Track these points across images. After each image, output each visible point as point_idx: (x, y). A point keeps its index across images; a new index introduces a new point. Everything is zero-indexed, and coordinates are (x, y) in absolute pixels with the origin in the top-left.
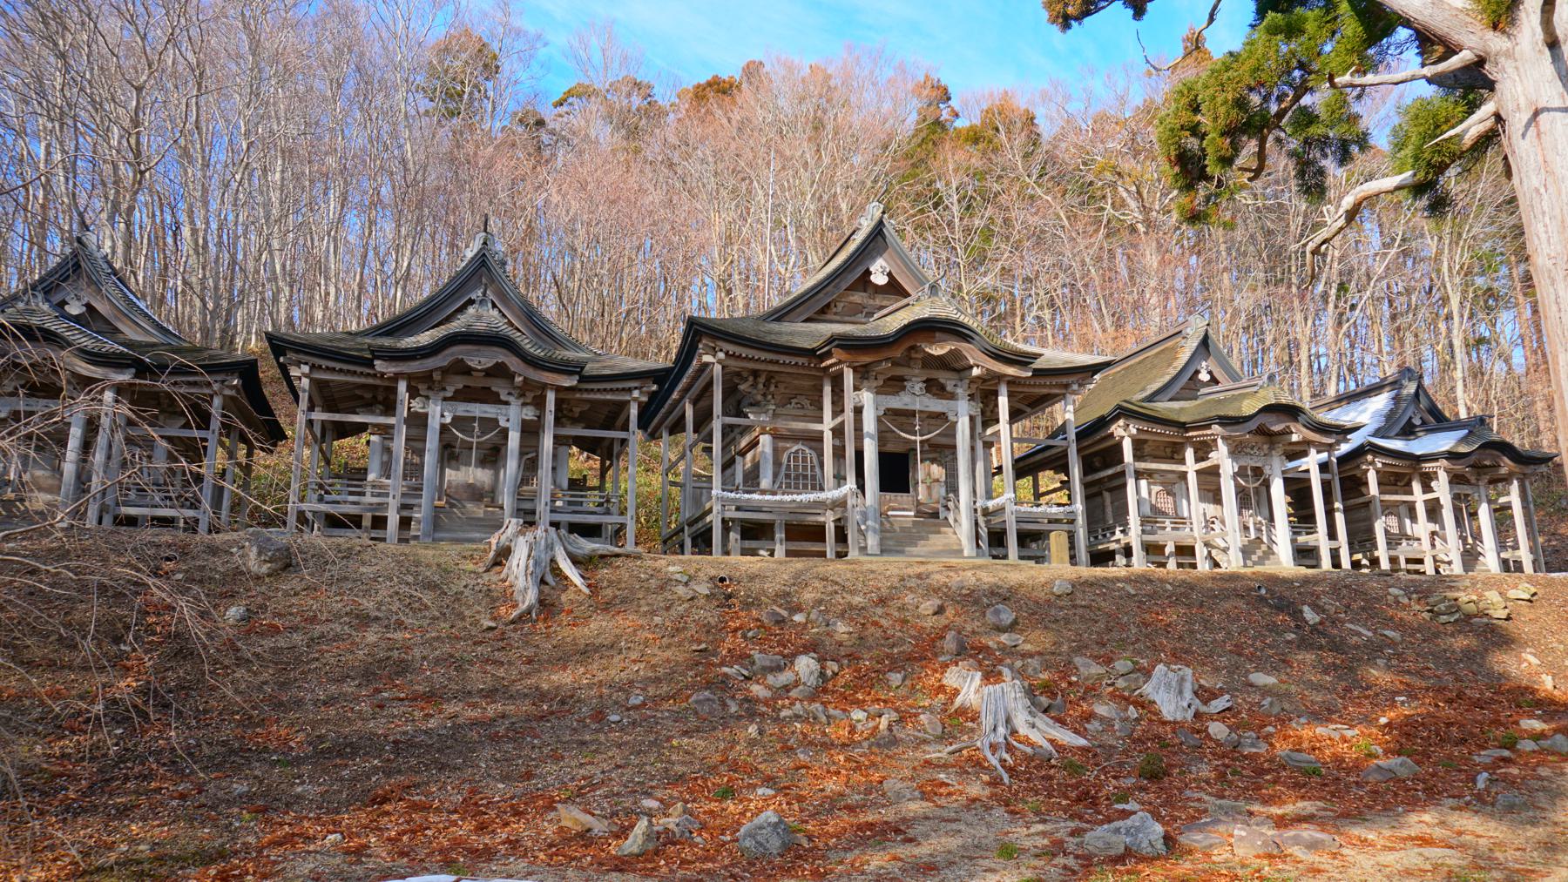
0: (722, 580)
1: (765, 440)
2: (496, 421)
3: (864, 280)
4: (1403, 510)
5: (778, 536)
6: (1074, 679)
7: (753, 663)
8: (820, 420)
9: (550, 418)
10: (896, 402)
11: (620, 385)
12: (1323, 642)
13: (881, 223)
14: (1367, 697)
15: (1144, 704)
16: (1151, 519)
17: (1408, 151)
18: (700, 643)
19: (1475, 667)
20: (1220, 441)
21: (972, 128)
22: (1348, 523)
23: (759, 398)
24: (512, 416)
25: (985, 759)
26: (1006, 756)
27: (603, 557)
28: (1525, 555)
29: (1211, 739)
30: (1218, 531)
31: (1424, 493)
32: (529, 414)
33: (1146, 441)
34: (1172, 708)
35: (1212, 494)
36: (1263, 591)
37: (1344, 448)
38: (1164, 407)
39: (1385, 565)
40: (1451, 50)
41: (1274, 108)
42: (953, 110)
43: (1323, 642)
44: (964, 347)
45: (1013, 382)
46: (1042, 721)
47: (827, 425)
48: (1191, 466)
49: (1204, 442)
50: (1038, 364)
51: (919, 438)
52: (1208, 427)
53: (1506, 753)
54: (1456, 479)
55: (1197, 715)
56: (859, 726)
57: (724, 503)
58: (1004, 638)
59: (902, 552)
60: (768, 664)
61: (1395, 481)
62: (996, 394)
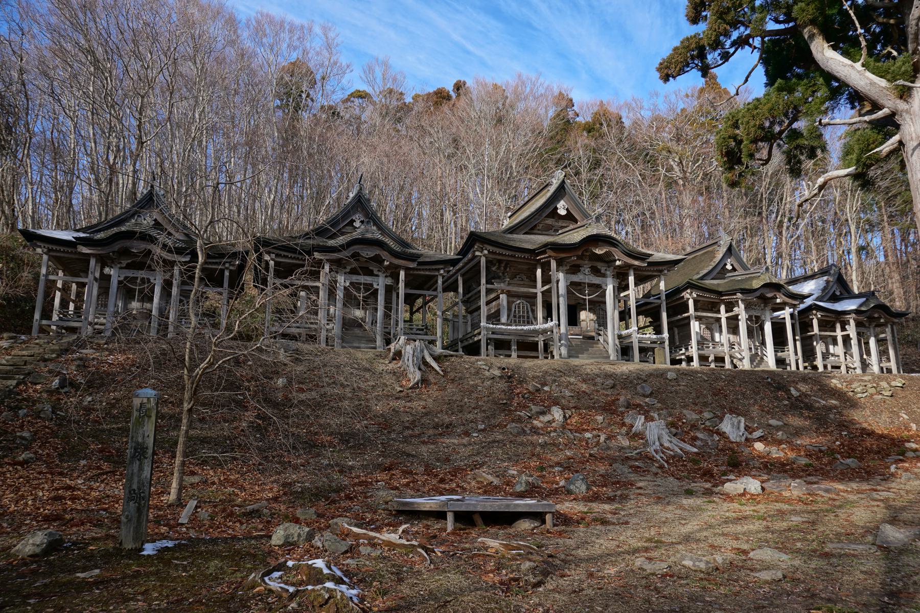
0: (504, 369)
1: (503, 297)
2: (372, 285)
3: (554, 213)
4: (830, 340)
5: (513, 347)
6: (684, 421)
7: (531, 410)
8: (535, 287)
9: (401, 285)
10: (576, 278)
11: (434, 267)
12: (802, 405)
13: (563, 182)
14: (828, 432)
15: (722, 434)
16: (701, 343)
17: (854, 156)
18: (503, 400)
19: (877, 419)
20: (740, 302)
21: (587, 123)
22: (803, 346)
23: (501, 274)
24: (380, 283)
25: (653, 456)
26: (663, 455)
27: (446, 356)
28: (893, 365)
29: (756, 450)
30: (737, 349)
31: (842, 331)
32: (389, 281)
33: (699, 301)
34: (735, 436)
35: (734, 329)
36: (769, 380)
37: (802, 306)
38: (709, 282)
39: (821, 369)
40: (876, 107)
41: (777, 129)
42: (575, 112)
43: (802, 405)
44: (613, 249)
45: (636, 269)
46: (675, 440)
47: (540, 288)
48: (723, 315)
49: (731, 302)
50: (650, 260)
51: (587, 297)
52: (735, 294)
53: (901, 457)
54: (859, 324)
55: (747, 439)
56: (590, 441)
57: (487, 329)
58: (647, 400)
59: (578, 357)
60: (538, 410)
61: (827, 325)
62: (627, 275)
